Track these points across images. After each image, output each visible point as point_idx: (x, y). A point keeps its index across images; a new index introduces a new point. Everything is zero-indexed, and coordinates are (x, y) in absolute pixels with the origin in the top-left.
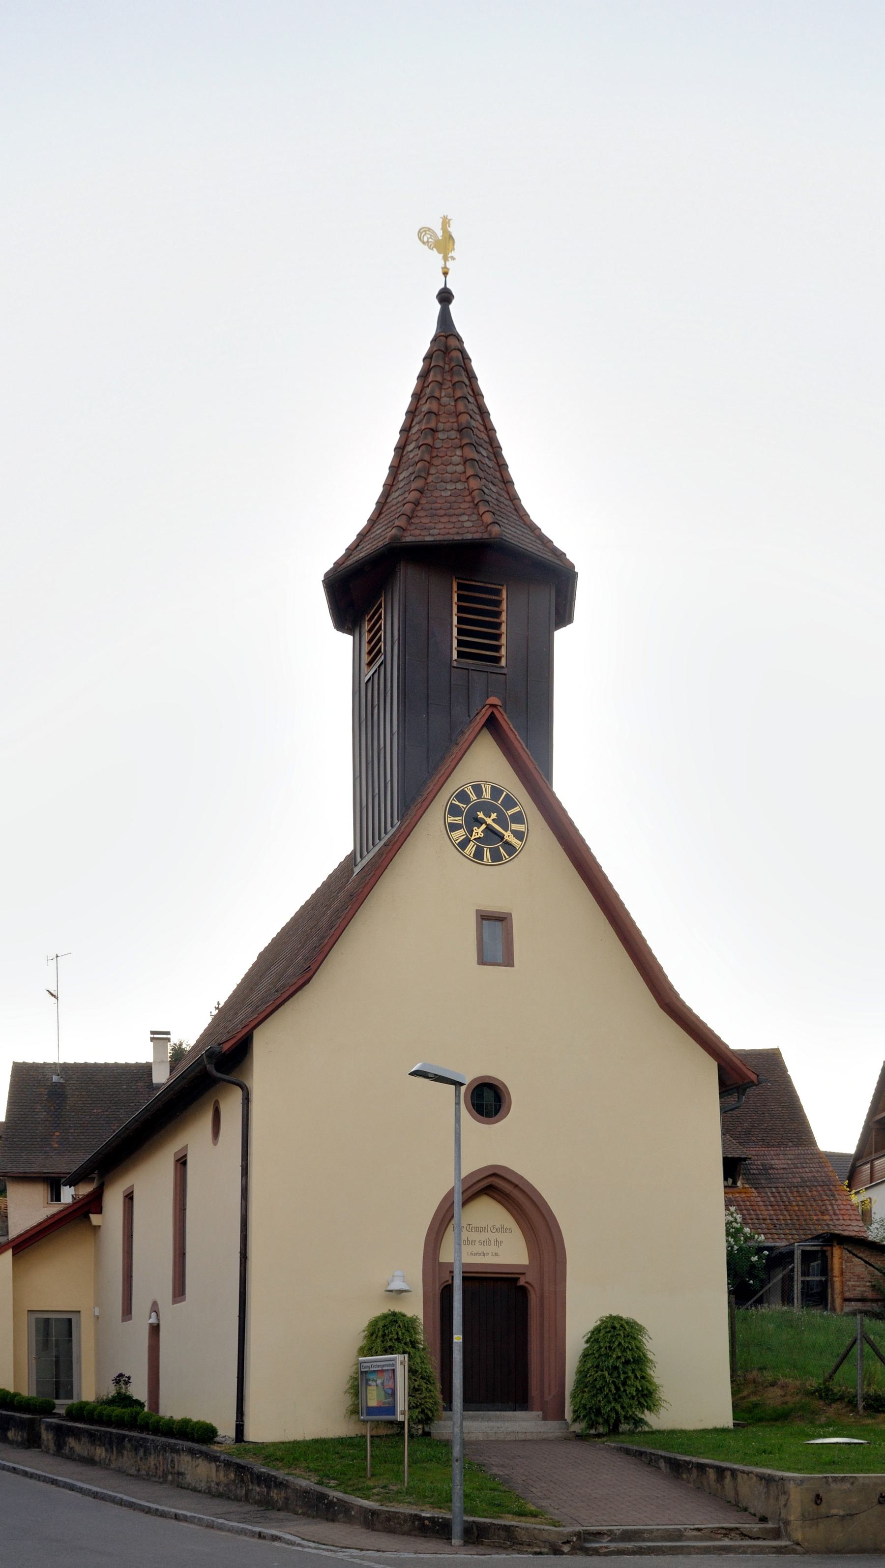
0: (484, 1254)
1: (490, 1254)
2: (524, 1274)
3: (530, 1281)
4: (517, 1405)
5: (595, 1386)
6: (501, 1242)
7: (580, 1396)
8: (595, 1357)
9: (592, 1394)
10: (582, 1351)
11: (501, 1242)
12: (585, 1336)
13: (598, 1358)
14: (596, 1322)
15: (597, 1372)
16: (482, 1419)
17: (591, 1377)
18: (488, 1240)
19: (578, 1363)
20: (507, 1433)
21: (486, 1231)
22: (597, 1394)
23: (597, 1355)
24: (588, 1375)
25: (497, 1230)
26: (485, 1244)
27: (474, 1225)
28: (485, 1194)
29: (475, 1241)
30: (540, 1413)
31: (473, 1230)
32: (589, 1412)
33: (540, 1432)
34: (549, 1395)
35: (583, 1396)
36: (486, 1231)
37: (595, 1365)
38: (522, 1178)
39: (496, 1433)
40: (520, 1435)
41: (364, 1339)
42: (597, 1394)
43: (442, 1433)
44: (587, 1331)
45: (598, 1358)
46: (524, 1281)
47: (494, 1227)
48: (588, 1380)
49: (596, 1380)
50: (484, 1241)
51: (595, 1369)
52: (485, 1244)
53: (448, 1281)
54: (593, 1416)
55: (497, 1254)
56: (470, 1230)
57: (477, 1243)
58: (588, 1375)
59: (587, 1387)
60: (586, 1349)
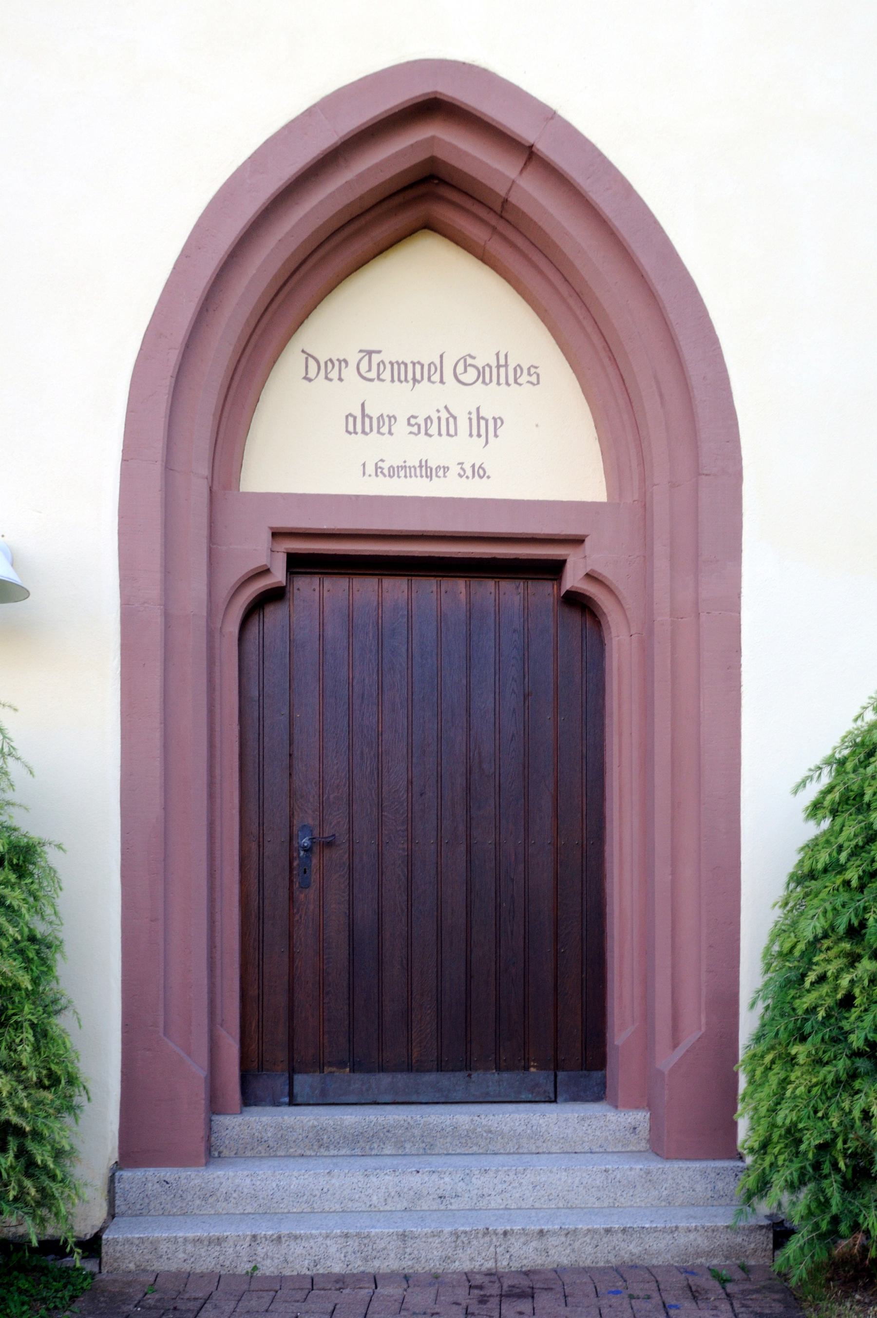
0: (427, 470)
1: (455, 470)
2: (578, 541)
3: (606, 572)
4: (561, 1075)
5: (840, 1038)
6: (498, 421)
7: (774, 1080)
8: (847, 883)
9: (827, 1073)
10: (797, 858)
11: (498, 421)
12: (803, 783)
13: (861, 888)
14: (860, 717)
15: (854, 959)
16: (400, 1144)
17: (825, 989)
18: (444, 415)
19: (778, 912)
20: (456, 1235)
21: (436, 377)
22: (853, 1075)
23: (853, 875)
24: (812, 977)
25: (481, 373)
26: (433, 430)
27: (386, 357)
28: (430, 226)
29: (392, 418)
30: (640, 1118)
31: (387, 375)
32: (817, 1166)
33: (608, 1231)
34: (675, 1045)
35: (784, 1082)
36: (436, 377)
37: (842, 929)
38: (549, 116)
39: (403, 1236)
40: (516, 1246)
41: (802, 849)
42: (853, 1075)
43: (155, 1244)
44: (817, 760)
45: (861, 888)
46: (582, 573)
47: (466, 361)
48: (808, 1000)
49: (848, 1001)
50: (428, 419)
51: (846, 946)
52: (433, 430)
53: (265, 572)
54: (833, 1189)
55: (479, 472)
56: (373, 374)
57: (401, 427)
58: (812, 977)
59: (803, 1039)
60: (813, 847)
